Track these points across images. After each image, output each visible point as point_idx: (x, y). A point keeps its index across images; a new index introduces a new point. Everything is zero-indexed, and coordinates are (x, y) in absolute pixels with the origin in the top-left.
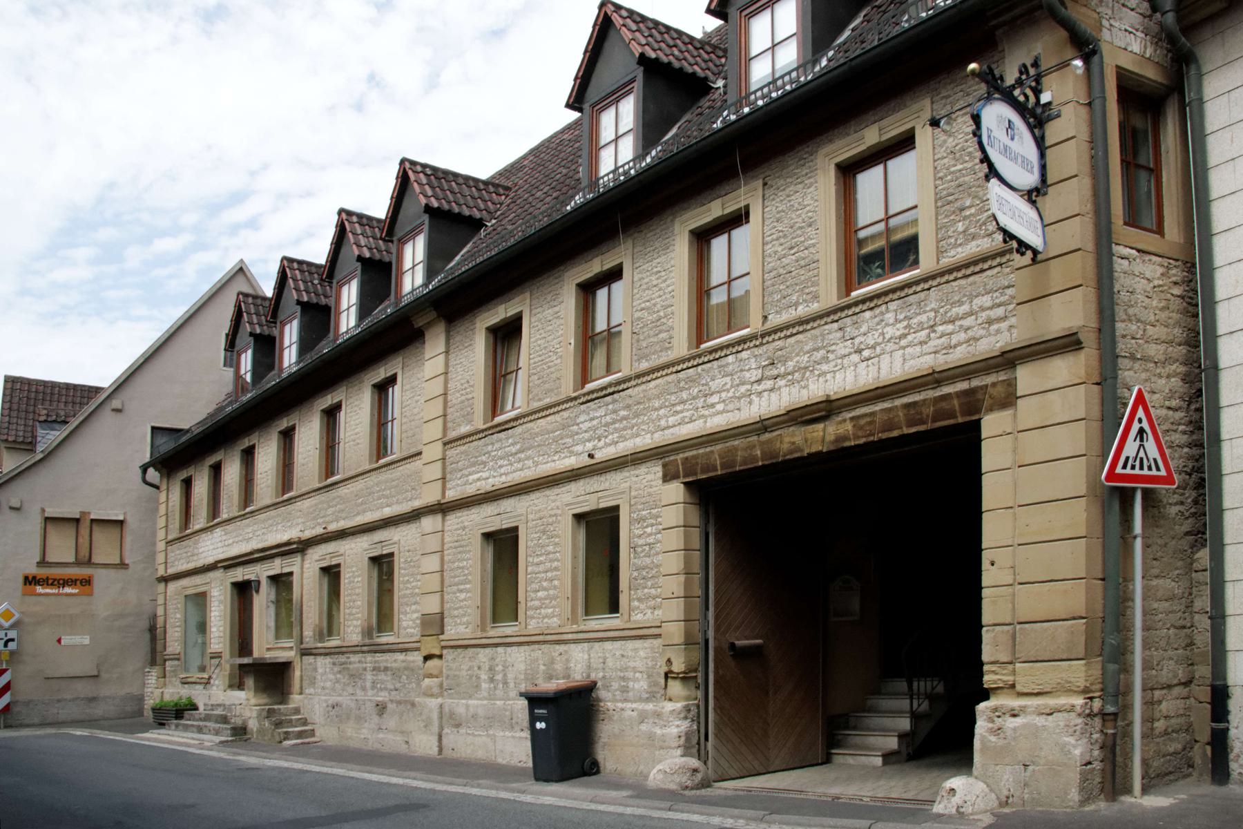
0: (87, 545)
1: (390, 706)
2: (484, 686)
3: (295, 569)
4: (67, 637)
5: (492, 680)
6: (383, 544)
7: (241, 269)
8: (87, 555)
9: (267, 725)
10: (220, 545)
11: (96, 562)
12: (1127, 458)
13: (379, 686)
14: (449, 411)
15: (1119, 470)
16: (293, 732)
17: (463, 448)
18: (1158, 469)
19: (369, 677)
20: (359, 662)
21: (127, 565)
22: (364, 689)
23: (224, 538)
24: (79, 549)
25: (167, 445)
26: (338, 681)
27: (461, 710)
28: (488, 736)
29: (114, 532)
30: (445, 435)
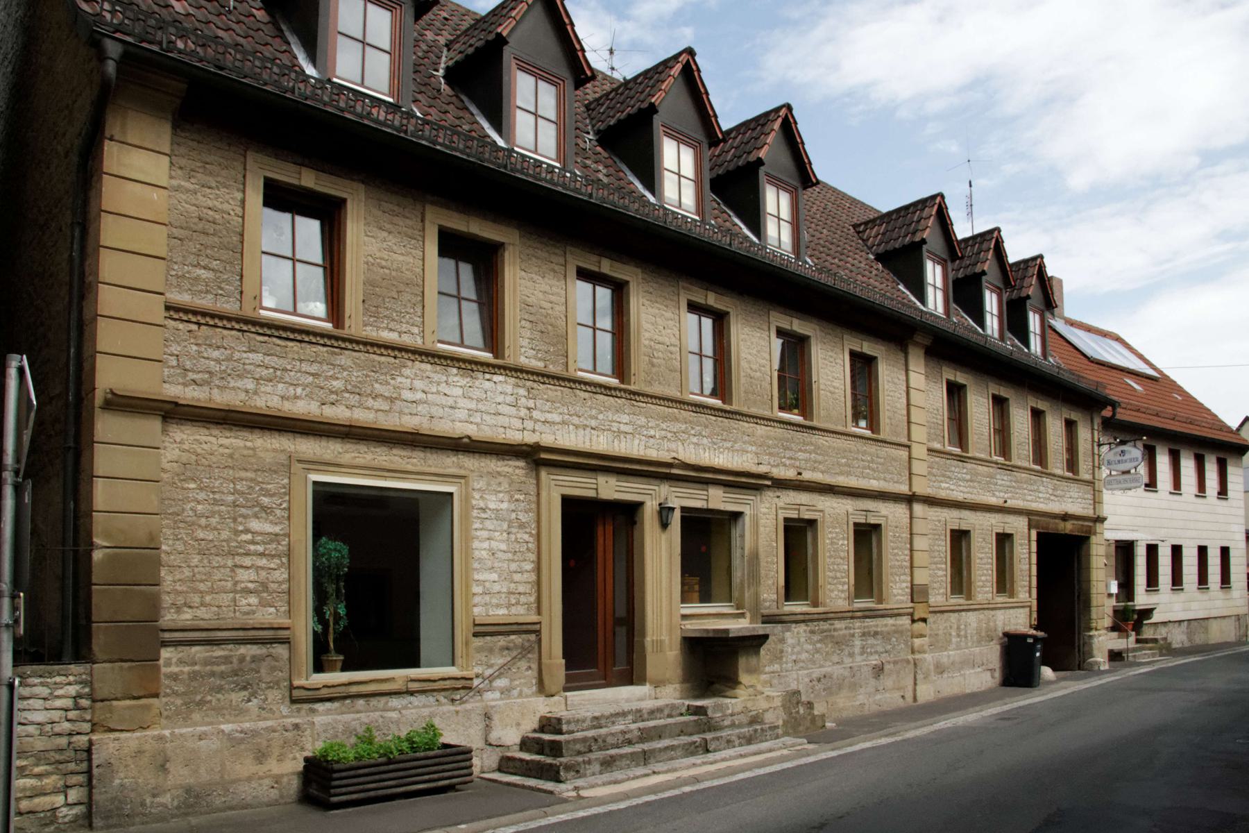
1: (887, 667)
2: (954, 640)
3: (746, 510)
5: (959, 636)
9: (802, 711)
13: (869, 650)
17: (937, 459)
19: (858, 643)
20: (846, 628)
22: (851, 655)
26: (817, 651)
27: (945, 660)
28: (961, 675)
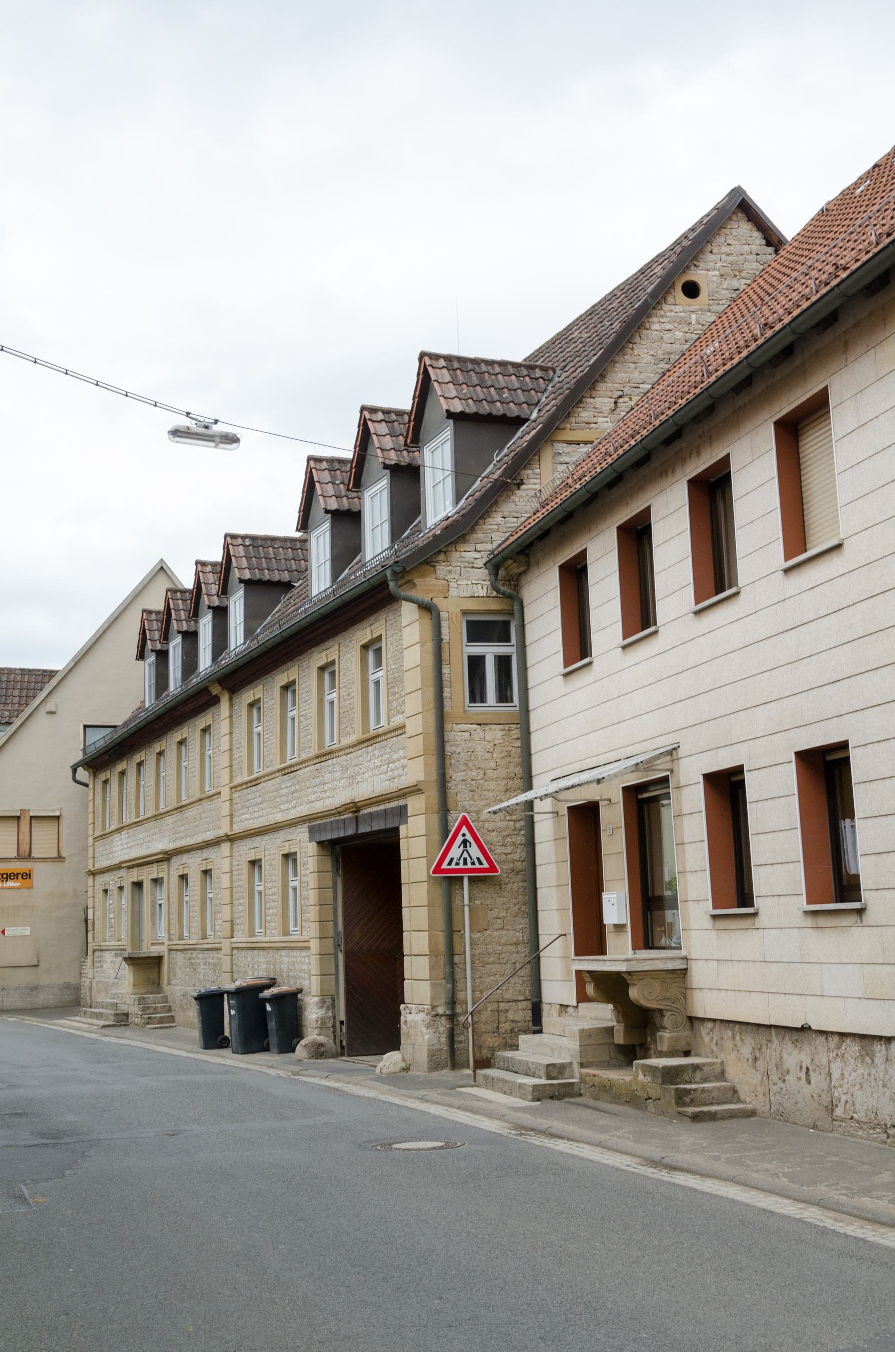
0: (28, 840)
4: (10, 928)
6: (208, 861)
7: (162, 568)
8: (27, 850)
10: (125, 846)
11: (36, 856)
12: (452, 860)
14: (234, 762)
15: (445, 866)
16: (155, 1018)
18: (481, 863)
21: (64, 858)
23: (128, 840)
24: (20, 843)
25: (98, 739)
29: (52, 827)
30: (231, 781)
